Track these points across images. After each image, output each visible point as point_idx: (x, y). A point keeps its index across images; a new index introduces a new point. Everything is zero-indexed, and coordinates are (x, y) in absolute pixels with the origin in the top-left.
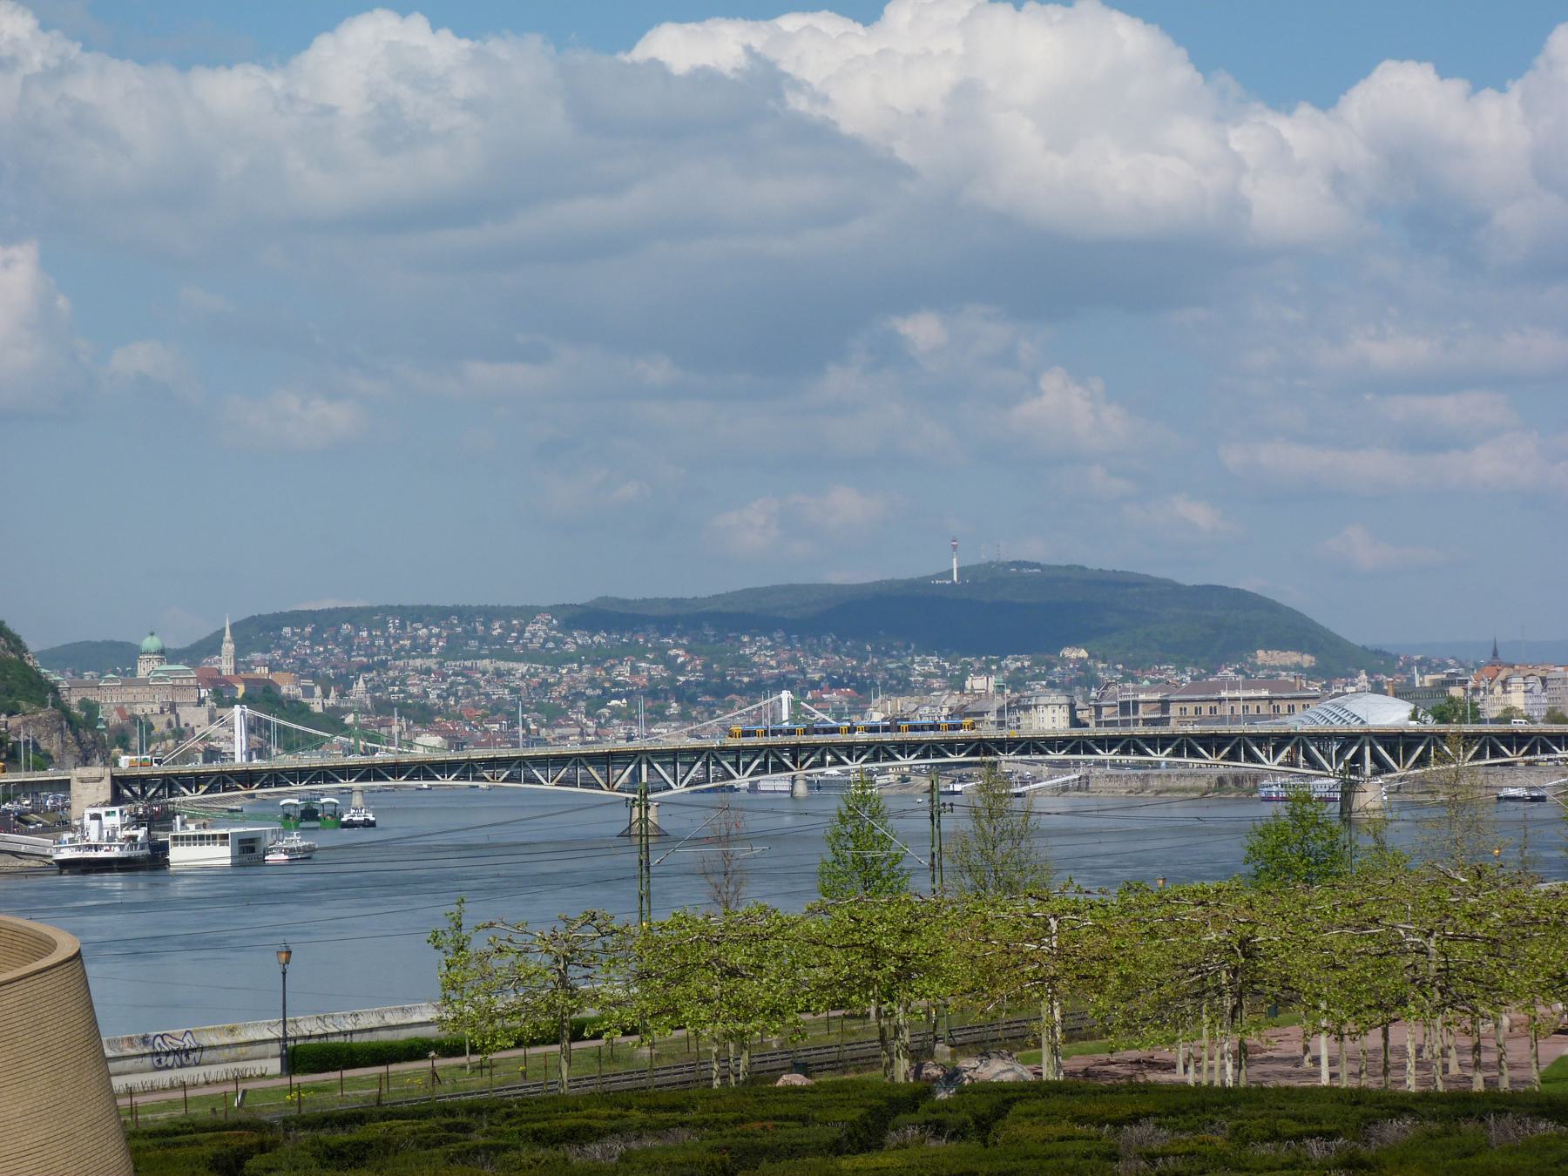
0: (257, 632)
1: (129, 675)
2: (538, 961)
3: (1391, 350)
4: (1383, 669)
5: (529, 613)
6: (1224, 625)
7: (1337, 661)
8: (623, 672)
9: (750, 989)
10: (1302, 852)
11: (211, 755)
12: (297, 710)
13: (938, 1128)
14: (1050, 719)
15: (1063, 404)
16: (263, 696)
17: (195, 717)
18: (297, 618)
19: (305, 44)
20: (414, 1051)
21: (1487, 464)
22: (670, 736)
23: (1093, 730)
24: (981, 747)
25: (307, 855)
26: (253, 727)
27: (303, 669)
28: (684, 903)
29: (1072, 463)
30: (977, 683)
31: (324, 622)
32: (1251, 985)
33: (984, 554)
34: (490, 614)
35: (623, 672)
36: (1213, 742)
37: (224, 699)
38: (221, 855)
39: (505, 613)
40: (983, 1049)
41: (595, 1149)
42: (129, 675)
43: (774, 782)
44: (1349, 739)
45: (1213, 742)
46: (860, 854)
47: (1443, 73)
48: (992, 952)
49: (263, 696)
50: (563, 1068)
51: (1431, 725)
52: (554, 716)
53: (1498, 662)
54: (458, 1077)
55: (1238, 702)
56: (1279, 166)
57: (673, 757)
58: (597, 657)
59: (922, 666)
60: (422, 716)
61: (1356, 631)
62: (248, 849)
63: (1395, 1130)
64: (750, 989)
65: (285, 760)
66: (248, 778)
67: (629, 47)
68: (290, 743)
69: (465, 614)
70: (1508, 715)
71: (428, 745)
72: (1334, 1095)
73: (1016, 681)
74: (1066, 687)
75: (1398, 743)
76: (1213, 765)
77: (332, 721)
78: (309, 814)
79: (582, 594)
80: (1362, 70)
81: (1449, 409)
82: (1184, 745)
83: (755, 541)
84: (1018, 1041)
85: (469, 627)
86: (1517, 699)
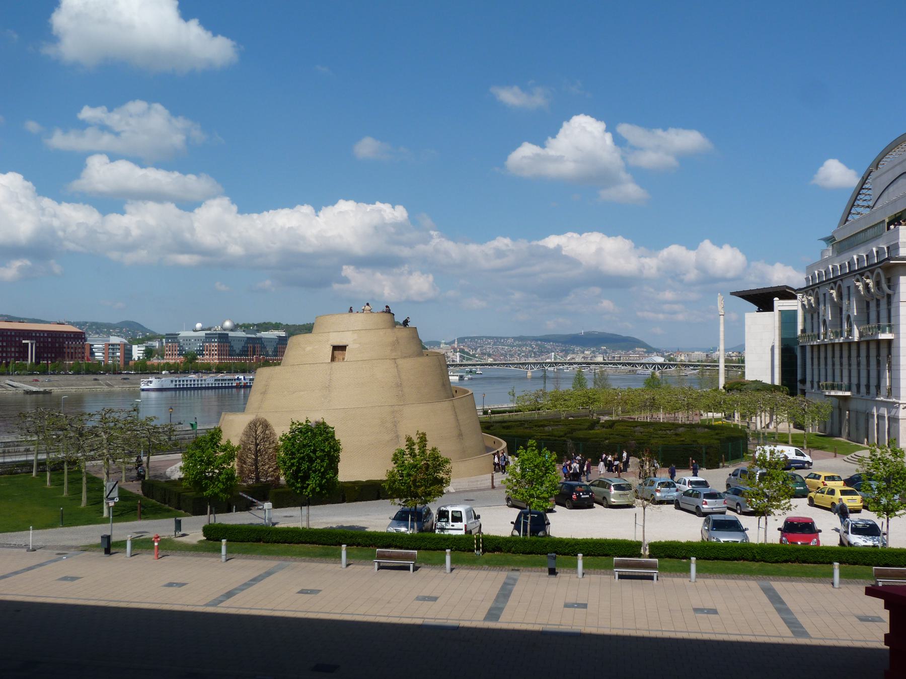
0: (461, 340)
1: (439, 347)
2: (532, 397)
3: (669, 295)
4: (659, 352)
5: (508, 338)
6: (629, 343)
7: (650, 350)
8: (524, 349)
9: (569, 403)
10: (652, 382)
11: (453, 361)
12: (468, 354)
13: (603, 427)
14: (600, 359)
15: (607, 304)
16: (462, 351)
17: (450, 354)
18: (467, 338)
19: (44, 196)
20: (504, 412)
21: (680, 317)
22: (531, 360)
23: (558, 361)
24: (614, 364)
25: (471, 379)
26: (460, 356)
27: (469, 347)
28: (550, 388)
29: (605, 314)
30: (586, 352)
31: (472, 339)
32: (653, 405)
33: (587, 330)
34: (501, 338)
35: (524, 349)
36: (629, 364)
37: (455, 351)
38: (457, 378)
39: (503, 338)
40: (603, 415)
41: (546, 428)
42: (439, 347)
43: (551, 369)
44: (653, 364)
45: (629, 364)
46: (579, 380)
47: (26, 178)
48: (609, 398)
49: (462, 351)
50: (535, 415)
51: (667, 362)
52: (512, 356)
53: (679, 351)
54: (520, 416)
55: (633, 357)
56: (651, 264)
57: (534, 364)
58: (520, 346)
59: (577, 349)
60: (490, 355)
61: (654, 346)
62: (461, 378)
63: (681, 429)
64: (569, 403)
65: (465, 362)
66: (461, 365)
67: (539, 239)
68: (468, 359)
69: (497, 338)
70: (681, 361)
71: (490, 360)
72: (663, 423)
73: (593, 352)
74: (602, 353)
75: (662, 365)
76: (629, 368)
77: (474, 356)
78: (471, 372)
79: (517, 334)
80: (667, 246)
81: (676, 307)
82: (624, 364)
83: (553, 326)
84: (610, 414)
85: (497, 340)
86: (683, 358)
